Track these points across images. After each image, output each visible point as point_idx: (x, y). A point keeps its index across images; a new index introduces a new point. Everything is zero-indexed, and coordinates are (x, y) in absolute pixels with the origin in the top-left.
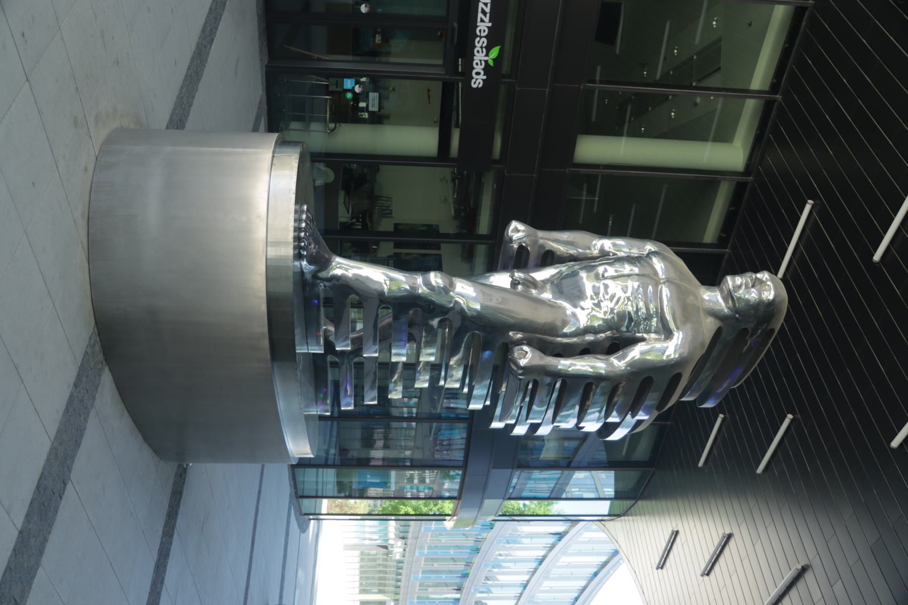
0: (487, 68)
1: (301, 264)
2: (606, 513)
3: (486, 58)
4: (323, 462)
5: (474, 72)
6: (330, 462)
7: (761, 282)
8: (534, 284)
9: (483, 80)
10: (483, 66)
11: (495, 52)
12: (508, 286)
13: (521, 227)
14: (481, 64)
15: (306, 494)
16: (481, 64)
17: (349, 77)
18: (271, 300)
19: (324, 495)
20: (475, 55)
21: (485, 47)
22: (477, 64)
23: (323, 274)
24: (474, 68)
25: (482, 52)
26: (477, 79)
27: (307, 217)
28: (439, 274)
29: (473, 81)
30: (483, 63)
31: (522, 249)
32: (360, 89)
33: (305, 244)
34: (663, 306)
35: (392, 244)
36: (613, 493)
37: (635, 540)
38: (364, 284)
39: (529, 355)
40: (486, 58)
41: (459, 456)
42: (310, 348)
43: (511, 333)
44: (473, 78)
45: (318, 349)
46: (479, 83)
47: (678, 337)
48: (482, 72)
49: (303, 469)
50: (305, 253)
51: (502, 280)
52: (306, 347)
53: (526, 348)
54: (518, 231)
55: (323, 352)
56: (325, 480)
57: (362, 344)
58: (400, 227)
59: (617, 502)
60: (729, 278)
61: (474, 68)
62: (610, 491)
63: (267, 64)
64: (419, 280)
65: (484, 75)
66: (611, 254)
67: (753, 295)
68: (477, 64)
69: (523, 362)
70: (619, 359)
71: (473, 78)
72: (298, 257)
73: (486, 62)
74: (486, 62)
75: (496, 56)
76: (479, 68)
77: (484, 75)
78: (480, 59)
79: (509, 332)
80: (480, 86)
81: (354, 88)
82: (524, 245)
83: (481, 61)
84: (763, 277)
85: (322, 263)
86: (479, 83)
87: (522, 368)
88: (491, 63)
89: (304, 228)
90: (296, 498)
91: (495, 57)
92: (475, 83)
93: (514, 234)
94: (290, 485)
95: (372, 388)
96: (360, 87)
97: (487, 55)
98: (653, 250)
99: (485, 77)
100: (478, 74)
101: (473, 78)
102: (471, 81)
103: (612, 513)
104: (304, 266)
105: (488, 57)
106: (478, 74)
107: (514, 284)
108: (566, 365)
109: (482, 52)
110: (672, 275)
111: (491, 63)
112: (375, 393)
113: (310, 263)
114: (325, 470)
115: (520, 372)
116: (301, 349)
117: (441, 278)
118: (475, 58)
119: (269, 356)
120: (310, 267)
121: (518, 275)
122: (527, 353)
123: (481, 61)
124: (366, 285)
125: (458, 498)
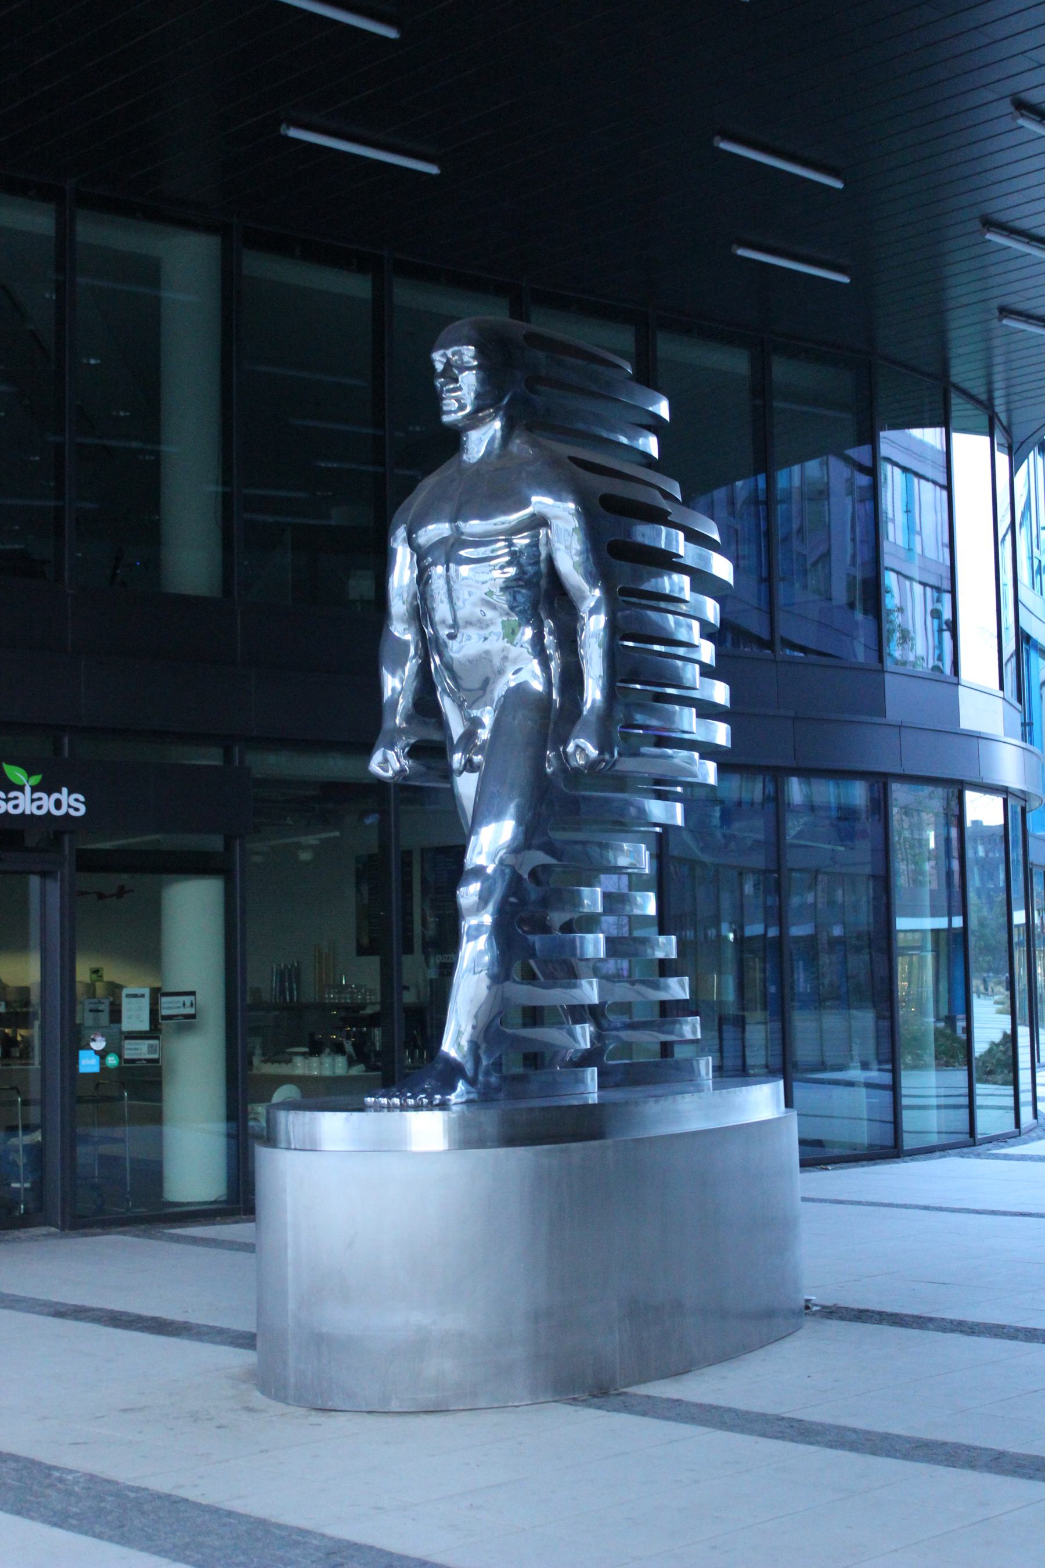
0: (48, 787)
1: (455, 1104)
2: (987, 439)
3: (28, 789)
4: (887, 1095)
5: (55, 812)
6: (886, 1078)
7: (448, 364)
8: (470, 735)
9: (69, 794)
10: (44, 795)
11: (16, 774)
12: (475, 777)
13: (377, 757)
14: (40, 799)
15: (966, 1127)
16: (40, 799)
17: (75, 1061)
18: (510, 1140)
19: (966, 1091)
20: (24, 812)
21: (6, 794)
22: (40, 807)
23: (469, 1068)
24: (49, 812)
25: (16, 798)
26: (69, 806)
27: (383, 1096)
28: (461, 889)
29: (72, 812)
30: (36, 795)
31: (414, 752)
32: (99, 1038)
33: (425, 1098)
34: (496, 530)
35: (407, 959)
36: (938, 430)
37: (1033, 385)
38: (481, 1006)
39: (582, 742)
40: (28, 789)
41: (858, 793)
42: (590, 1090)
43: (549, 770)
44: (67, 813)
45: (592, 1074)
46: (77, 800)
47: (541, 502)
48: (55, 796)
49: (905, 1135)
50: (438, 1097)
51: (467, 785)
52: (591, 1095)
53: (571, 748)
54: (386, 761)
55: (596, 1068)
56: (934, 1092)
57: (583, 1006)
58: (365, 941)
59: (954, 423)
60: (446, 419)
61: (49, 812)
62: (931, 436)
63: (57, 1227)
64: (469, 923)
65: (60, 792)
66: (415, 603)
67: (469, 381)
68: (40, 807)
69: (593, 752)
70: (584, 598)
71: (67, 813)
72: (443, 1106)
73: (34, 789)
74: (34, 789)
75: (22, 771)
76: (48, 803)
77: (60, 792)
78: (29, 801)
79: (546, 774)
80: (82, 798)
81: (97, 1052)
82: (407, 750)
83: (33, 801)
84: (441, 362)
85: (452, 1071)
86: (77, 800)
87: (601, 753)
88: (36, 779)
89: (400, 1099)
90: (974, 1145)
91: (26, 775)
92: (77, 810)
93: (390, 768)
94: (941, 1157)
95: (666, 988)
96: (94, 1040)
97: (21, 789)
98: (405, 534)
99: (65, 790)
100: (58, 804)
101: (67, 814)
102: (56, 816)
103: (987, 429)
104: (459, 1100)
105: (25, 785)
106: (58, 804)
107: (470, 766)
108: (593, 692)
109: (16, 798)
110: (448, 508)
111: (36, 779)
112: (673, 982)
113: (453, 1088)
114: (904, 1092)
115: (607, 757)
116: (593, 1098)
117: (468, 885)
118: (28, 812)
119: (595, 1143)
120: (459, 1089)
121: (457, 759)
122: (577, 747)
123: (33, 801)
124: (483, 1004)
125: (960, 787)
